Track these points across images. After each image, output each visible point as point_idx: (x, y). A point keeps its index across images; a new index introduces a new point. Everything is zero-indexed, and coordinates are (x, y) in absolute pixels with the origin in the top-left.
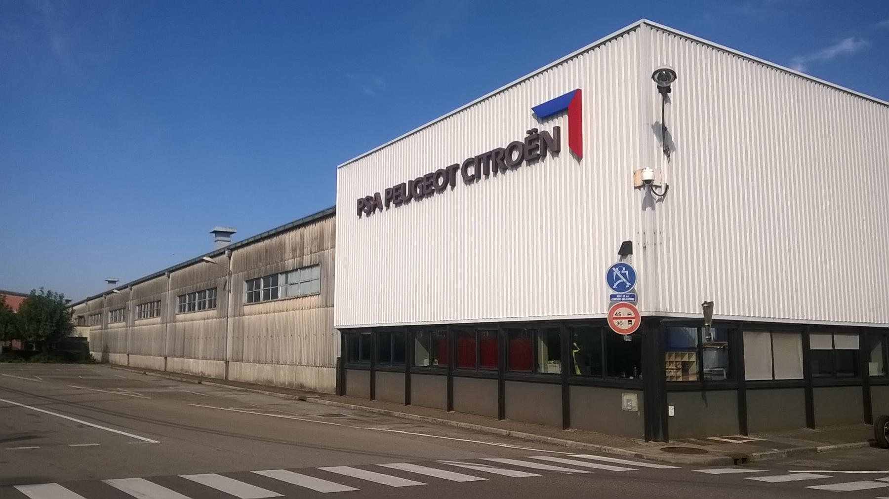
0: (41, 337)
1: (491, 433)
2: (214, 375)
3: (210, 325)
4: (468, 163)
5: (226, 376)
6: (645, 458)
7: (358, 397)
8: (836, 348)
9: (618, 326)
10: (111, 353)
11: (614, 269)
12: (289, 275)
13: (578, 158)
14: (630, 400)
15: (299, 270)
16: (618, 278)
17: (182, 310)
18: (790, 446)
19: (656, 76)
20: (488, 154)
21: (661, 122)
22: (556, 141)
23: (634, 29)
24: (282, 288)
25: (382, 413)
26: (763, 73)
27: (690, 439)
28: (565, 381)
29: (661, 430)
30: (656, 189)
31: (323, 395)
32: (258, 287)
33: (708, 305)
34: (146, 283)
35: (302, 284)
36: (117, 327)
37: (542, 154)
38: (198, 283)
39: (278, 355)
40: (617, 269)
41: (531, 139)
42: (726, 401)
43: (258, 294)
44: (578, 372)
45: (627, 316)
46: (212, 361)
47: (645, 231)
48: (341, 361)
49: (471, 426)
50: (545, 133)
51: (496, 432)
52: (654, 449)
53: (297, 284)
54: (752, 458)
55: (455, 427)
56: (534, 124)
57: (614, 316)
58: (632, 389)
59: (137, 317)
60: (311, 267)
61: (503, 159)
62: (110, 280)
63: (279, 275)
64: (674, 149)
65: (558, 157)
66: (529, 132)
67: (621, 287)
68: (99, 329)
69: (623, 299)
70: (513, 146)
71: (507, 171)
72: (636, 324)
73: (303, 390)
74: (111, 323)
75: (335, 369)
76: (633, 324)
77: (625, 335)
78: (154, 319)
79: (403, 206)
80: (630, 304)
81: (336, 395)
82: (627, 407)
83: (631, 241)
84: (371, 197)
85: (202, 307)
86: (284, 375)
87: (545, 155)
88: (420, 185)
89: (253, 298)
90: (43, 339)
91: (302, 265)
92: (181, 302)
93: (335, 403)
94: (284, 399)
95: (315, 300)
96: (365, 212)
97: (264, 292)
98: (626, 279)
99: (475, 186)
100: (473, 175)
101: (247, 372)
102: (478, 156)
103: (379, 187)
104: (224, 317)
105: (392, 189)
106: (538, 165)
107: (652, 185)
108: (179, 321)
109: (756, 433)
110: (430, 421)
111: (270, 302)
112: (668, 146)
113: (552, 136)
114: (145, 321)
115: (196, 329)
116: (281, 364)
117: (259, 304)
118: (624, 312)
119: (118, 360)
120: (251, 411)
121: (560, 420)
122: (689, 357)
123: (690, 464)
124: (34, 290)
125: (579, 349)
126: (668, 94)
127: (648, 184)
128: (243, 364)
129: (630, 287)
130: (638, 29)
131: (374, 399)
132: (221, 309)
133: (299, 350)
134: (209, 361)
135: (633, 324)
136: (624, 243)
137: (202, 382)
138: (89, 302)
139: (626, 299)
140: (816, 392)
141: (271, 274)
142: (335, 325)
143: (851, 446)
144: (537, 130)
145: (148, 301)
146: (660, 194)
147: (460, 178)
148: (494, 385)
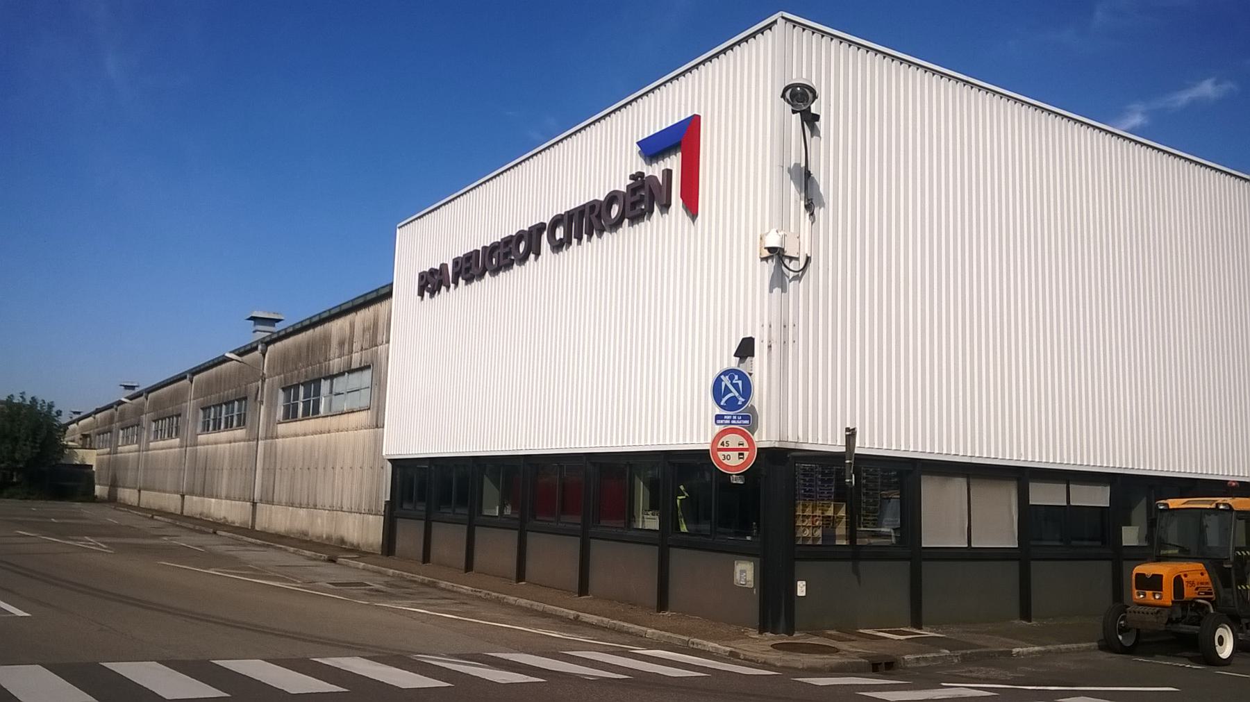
0: (18, 462)
2: (239, 522)
3: (236, 451)
4: (557, 221)
5: (252, 524)
6: (742, 657)
7: (409, 559)
8: (1072, 504)
9: (724, 461)
10: (120, 487)
11: (722, 377)
12: (335, 380)
14: (745, 571)
15: (346, 374)
16: (728, 391)
17: (206, 429)
18: (971, 646)
19: (788, 95)
20: (581, 209)
21: (803, 165)
22: (664, 189)
23: (769, 27)
25: (426, 582)
26: (1057, 125)
27: (829, 632)
28: (665, 541)
29: (783, 618)
30: (790, 262)
32: (296, 397)
33: (850, 433)
34: (165, 389)
36: (128, 450)
37: (647, 209)
38: (225, 390)
39: (315, 495)
40: (727, 377)
41: (634, 186)
42: (895, 576)
43: (296, 407)
46: (237, 502)
47: (771, 322)
48: (390, 505)
49: (532, 605)
51: (562, 614)
52: (760, 645)
53: (343, 394)
54: (902, 663)
55: (512, 605)
56: (639, 165)
57: (720, 446)
59: (152, 438)
61: (599, 217)
62: (125, 384)
63: (322, 380)
64: (822, 204)
65: (668, 213)
66: (632, 177)
67: (732, 405)
68: (108, 454)
69: (734, 422)
70: (613, 198)
71: (605, 233)
72: (750, 458)
73: (344, 546)
74: (122, 445)
75: (382, 518)
76: (745, 457)
77: (732, 475)
78: (173, 440)
79: (475, 283)
80: (742, 428)
81: (382, 554)
82: (740, 580)
83: (753, 337)
84: (436, 270)
85: (229, 426)
86: (321, 525)
87: (652, 211)
88: (496, 253)
89: (291, 414)
90: (21, 466)
91: (350, 367)
92: (204, 417)
93: (370, 566)
94: (310, 558)
95: (363, 417)
96: (428, 291)
97: (303, 405)
98: (739, 392)
99: (564, 253)
100: (561, 239)
101: (277, 518)
102: (568, 212)
103: (444, 255)
104: (253, 440)
105: (462, 258)
106: (642, 224)
107: (783, 255)
108: (200, 445)
109: (935, 625)
110: (483, 595)
112: (812, 199)
113: (661, 181)
114: (161, 443)
115: (220, 455)
116: (319, 509)
117: (296, 421)
118: (734, 440)
119: (127, 497)
120: (229, 573)
121: (653, 600)
122: (836, 510)
123: (802, 669)
124: (12, 395)
125: (686, 494)
126: (817, 123)
127: (777, 254)
128: (273, 507)
129: (744, 403)
130: (775, 27)
131: (429, 561)
132: (251, 428)
133: (340, 489)
134: (233, 502)
135: (745, 457)
136: (743, 339)
137: (218, 532)
138: (98, 416)
139: (738, 422)
141: (312, 379)
142: (384, 454)
143: (1067, 649)
144: (643, 174)
145: (165, 415)
146: (798, 270)
147: (547, 247)
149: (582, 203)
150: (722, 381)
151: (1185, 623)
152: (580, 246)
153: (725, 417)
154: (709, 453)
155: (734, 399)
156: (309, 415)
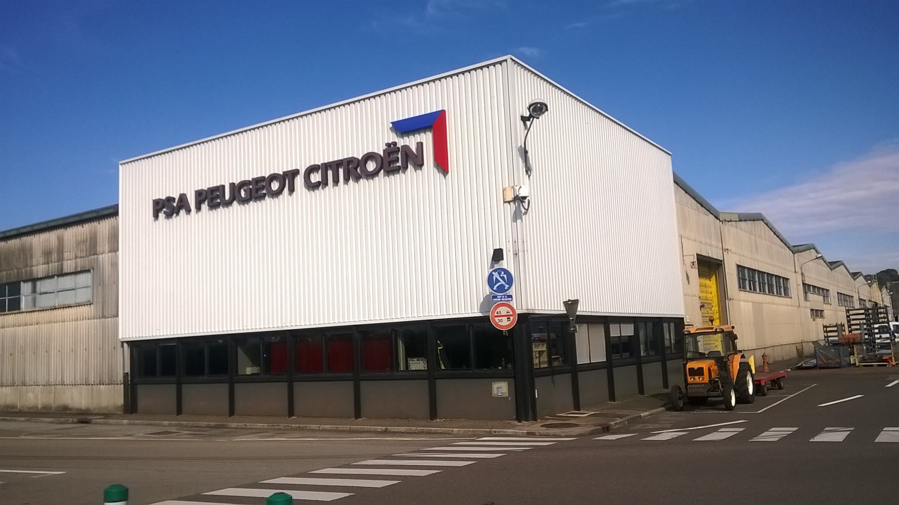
1: (363, 431)
4: (312, 169)
6: (537, 434)
8: (622, 335)
11: (493, 273)
13: (444, 171)
15: (56, 277)
16: (497, 280)
20: (338, 162)
21: (523, 146)
24: (25, 299)
28: (431, 376)
31: (107, 415)
35: (60, 293)
40: (497, 273)
41: (390, 151)
44: (443, 367)
45: (506, 314)
49: (337, 428)
50: (406, 148)
52: (526, 426)
56: (392, 138)
57: (496, 314)
58: (503, 378)
60: (76, 273)
63: (22, 283)
65: (421, 170)
69: (503, 299)
70: (370, 156)
71: (361, 179)
72: (514, 320)
73: (68, 412)
75: (122, 385)
76: (511, 320)
79: (221, 210)
87: (407, 168)
98: (505, 281)
99: (320, 192)
102: (325, 164)
111: (6, 315)
129: (509, 288)
135: (511, 320)
139: (506, 299)
140: (616, 371)
148: (349, 386)
149: (341, 158)
150: (494, 275)
151: (711, 391)
152: (337, 188)
153: (498, 297)
154: (489, 318)
155: (502, 286)
156: (5, 311)
